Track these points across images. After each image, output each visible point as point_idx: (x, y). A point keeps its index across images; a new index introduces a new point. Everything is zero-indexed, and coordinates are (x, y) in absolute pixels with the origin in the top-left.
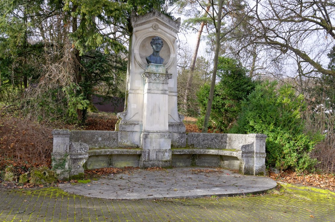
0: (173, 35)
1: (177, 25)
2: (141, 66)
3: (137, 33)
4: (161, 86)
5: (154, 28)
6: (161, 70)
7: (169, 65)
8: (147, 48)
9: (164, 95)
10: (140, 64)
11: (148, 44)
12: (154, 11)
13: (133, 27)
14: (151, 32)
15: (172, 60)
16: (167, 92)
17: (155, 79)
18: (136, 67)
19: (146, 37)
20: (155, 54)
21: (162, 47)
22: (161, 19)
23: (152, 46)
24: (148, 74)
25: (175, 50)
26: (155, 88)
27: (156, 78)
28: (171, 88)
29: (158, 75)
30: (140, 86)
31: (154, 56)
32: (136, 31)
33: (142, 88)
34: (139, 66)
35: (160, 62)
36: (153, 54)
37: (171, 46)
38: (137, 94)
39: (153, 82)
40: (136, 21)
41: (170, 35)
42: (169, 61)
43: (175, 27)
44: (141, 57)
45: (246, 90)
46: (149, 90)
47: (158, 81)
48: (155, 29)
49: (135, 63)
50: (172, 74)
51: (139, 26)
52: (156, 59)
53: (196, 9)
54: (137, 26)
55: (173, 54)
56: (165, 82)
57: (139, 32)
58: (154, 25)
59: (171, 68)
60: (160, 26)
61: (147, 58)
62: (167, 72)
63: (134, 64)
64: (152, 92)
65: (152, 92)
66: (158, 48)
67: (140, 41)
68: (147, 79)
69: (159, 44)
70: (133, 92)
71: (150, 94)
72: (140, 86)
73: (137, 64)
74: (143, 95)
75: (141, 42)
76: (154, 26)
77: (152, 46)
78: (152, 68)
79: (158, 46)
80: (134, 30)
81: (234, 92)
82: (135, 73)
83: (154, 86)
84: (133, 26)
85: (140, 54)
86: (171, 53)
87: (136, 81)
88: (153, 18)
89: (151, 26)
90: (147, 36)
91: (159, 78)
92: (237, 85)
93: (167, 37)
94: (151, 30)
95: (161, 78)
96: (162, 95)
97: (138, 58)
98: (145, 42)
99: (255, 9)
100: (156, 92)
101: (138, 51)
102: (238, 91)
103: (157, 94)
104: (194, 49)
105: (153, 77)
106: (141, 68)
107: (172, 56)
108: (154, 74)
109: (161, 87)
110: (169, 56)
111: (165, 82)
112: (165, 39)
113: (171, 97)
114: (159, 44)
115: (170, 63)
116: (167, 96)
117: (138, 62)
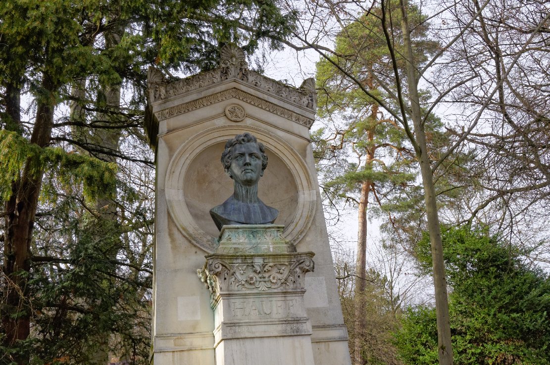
0: (296, 132)
1: (305, 100)
2: (194, 242)
3: (171, 136)
4: (280, 303)
5: (229, 116)
6: (269, 243)
7: (299, 228)
8: (216, 186)
9: (296, 339)
10: (190, 235)
11: (216, 170)
12: (223, 66)
13: (159, 120)
14: (223, 128)
15: (305, 214)
16: (307, 327)
17: (252, 278)
18: (175, 248)
19: (205, 146)
20: (243, 191)
21: (264, 167)
22: (250, 87)
23: (228, 168)
24: (220, 265)
25: (311, 178)
26: (254, 316)
27: (252, 275)
28: (317, 311)
29: (258, 261)
30: (198, 317)
31: (238, 200)
32: (170, 131)
33: (203, 327)
34: (186, 243)
35: (261, 218)
36: (236, 195)
37: (297, 166)
38: (185, 353)
39: (245, 291)
40: (166, 99)
41: (288, 132)
42: (298, 216)
43: (300, 107)
44: (196, 216)
45: (539, 305)
46: (228, 325)
47: (263, 287)
48: (234, 119)
49: (171, 235)
50: (312, 254)
51: (180, 113)
52: (248, 207)
53: (346, 161)
54: (171, 114)
55: (306, 192)
56: (291, 286)
57: (180, 132)
58: (229, 108)
59: (308, 239)
60: (250, 109)
61: (216, 211)
62: (293, 247)
63: (168, 240)
64: (244, 332)
65: (244, 332)
66: (249, 167)
67: (185, 160)
68: (218, 284)
69: (251, 155)
70: (170, 344)
71: (234, 345)
72: (198, 317)
73: (180, 236)
74: (210, 352)
75: (188, 162)
76: (231, 112)
77: (228, 168)
78: (237, 240)
79: (248, 161)
80: (163, 127)
81: (505, 317)
82: (176, 271)
83: (249, 309)
84: (156, 115)
85: (189, 205)
86: (300, 187)
87: (181, 301)
88: (223, 87)
89: (220, 110)
90: (209, 143)
91: (266, 275)
92: (509, 293)
93: (279, 140)
94: (221, 122)
95: (274, 273)
96: (288, 341)
97: (183, 217)
98: (206, 166)
99: (497, 96)
100: (259, 330)
101: (181, 191)
102: (516, 311)
103: (266, 340)
104: (355, 248)
105: (241, 274)
106: (194, 249)
107: (305, 197)
108: (245, 257)
109: (276, 307)
110: (294, 200)
111: (290, 287)
112: (271, 145)
113: (322, 346)
114: (251, 155)
115: (301, 223)
116: (306, 342)
117: (184, 229)
